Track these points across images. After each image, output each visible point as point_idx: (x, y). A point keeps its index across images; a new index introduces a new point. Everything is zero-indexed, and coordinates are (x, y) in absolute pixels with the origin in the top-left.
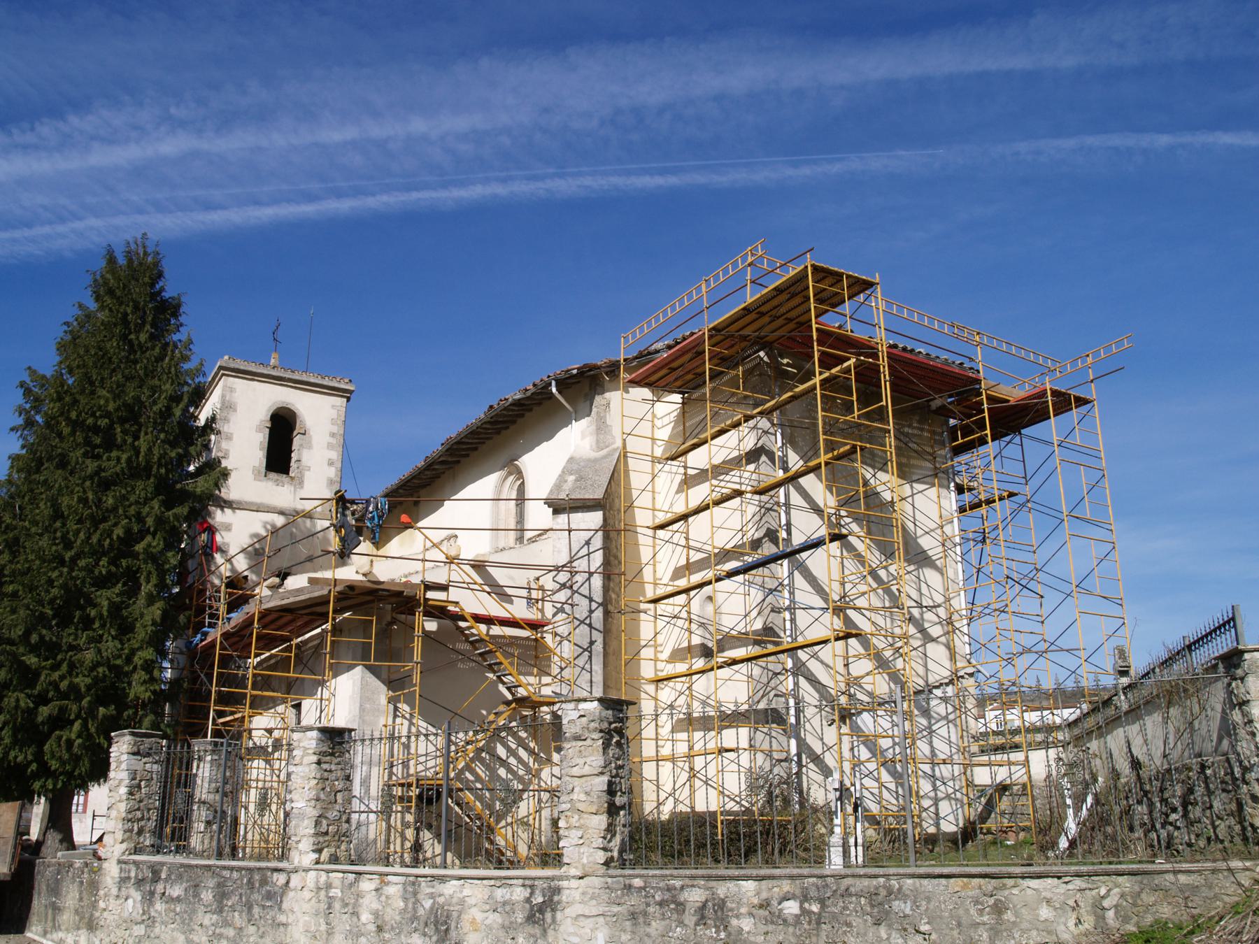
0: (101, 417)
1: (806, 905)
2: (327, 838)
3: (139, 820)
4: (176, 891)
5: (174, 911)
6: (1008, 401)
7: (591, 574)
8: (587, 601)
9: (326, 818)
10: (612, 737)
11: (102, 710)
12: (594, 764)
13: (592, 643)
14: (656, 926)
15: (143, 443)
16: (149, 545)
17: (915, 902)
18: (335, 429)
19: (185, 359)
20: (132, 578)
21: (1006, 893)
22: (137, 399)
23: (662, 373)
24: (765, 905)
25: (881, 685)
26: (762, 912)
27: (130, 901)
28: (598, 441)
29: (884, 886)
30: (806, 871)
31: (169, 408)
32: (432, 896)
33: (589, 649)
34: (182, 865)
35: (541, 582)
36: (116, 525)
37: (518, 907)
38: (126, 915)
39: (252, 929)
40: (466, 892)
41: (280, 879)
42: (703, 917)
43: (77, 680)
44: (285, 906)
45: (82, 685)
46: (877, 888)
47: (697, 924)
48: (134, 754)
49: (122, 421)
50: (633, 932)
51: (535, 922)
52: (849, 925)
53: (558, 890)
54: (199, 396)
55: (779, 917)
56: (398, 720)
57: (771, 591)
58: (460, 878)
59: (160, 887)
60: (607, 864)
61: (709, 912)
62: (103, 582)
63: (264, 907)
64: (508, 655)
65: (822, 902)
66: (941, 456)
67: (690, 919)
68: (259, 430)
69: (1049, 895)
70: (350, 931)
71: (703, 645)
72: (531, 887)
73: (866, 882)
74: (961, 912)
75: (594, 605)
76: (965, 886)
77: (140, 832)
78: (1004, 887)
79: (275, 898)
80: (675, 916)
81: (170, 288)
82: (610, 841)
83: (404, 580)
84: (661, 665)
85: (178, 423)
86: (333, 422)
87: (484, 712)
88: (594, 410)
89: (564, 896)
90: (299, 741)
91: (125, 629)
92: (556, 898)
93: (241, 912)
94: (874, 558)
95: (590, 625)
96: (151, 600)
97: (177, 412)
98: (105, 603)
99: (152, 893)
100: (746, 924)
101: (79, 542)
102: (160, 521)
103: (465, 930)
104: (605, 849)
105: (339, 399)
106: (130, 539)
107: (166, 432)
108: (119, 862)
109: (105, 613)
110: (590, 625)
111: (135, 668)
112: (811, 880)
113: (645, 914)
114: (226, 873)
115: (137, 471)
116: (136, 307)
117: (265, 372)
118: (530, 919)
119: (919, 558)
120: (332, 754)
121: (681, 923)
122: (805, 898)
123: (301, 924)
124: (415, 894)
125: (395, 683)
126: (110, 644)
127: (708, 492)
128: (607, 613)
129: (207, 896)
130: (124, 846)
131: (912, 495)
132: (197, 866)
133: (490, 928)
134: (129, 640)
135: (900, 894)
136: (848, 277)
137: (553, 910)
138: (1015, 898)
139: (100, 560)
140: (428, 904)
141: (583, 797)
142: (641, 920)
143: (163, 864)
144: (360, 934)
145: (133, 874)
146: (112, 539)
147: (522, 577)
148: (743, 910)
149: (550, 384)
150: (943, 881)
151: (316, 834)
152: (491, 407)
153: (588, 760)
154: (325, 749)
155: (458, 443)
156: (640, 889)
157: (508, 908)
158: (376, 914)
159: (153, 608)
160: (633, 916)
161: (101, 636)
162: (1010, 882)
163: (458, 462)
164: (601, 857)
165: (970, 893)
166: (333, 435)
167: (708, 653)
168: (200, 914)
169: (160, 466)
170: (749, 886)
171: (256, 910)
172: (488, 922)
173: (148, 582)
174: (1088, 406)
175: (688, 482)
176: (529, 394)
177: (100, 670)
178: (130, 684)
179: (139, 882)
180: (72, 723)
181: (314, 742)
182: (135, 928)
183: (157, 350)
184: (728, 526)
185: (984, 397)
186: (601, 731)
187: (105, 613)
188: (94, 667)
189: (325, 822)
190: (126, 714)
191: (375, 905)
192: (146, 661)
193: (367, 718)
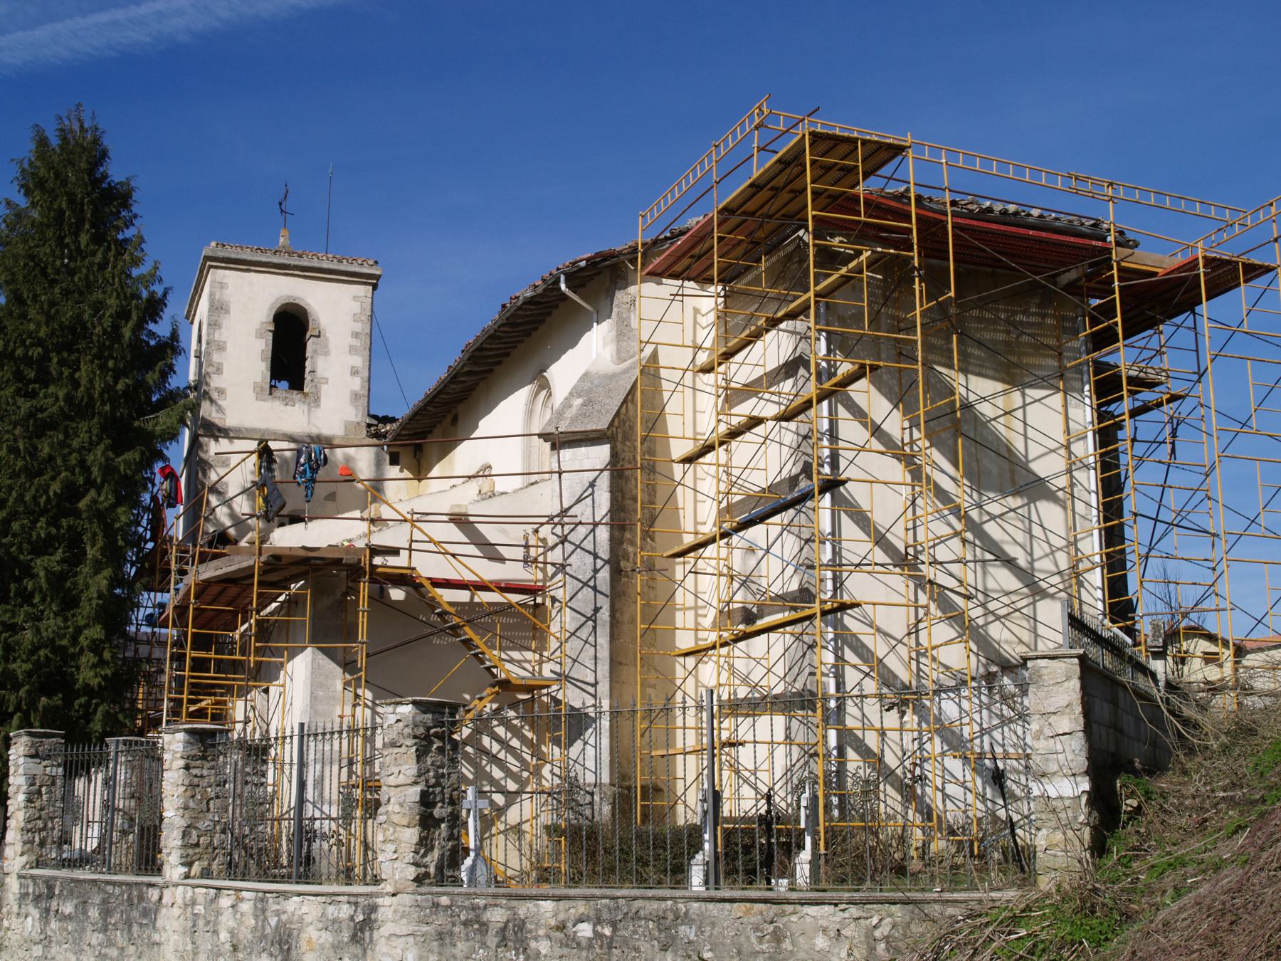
0: (32, 345)
1: (599, 928)
2: (197, 850)
3: (40, 830)
4: (68, 908)
5: (66, 929)
6: (1155, 274)
7: (595, 524)
8: (591, 558)
9: (196, 828)
10: (432, 743)
11: (44, 700)
12: (408, 773)
13: (597, 610)
14: (461, 947)
15: (83, 374)
16: (94, 502)
17: (700, 927)
18: (358, 327)
19: (136, 262)
20: (75, 544)
21: (786, 919)
22: (78, 317)
23: (684, 261)
24: (561, 927)
25: (958, 656)
26: (559, 935)
27: (29, 919)
28: (618, 351)
29: (671, 910)
30: (597, 892)
31: (116, 328)
32: (278, 913)
33: (593, 618)
34: (73, 880)
35: (541, 535)
36: (53, 478)
37: (344, 926)
38: (26, 934)
39: (132, 949)
40: (305, 909)
41: (154, 894)
42: (504, 938)
43: (14, 666)
44: (159, 924)
45: (19, 671)
46: (664, 912)
47: (498, 946)
48: (31, 756)
49: (59, 349)
50: (440, 954)
51: (357, 942)
52: (637, 950)
53: (374, 908)
54: (154, 307)
55: (573, 940)
56: (359, 710)
57: (807, 541)
58: (299, 895)
59: (54, 904)
60: (419, 880)
61: (510, 934)
62: (41, 548)
63: (141, 925)
64: (482, 630)
65: (614, 925)
66: (1072, 349)
67: (492, 941)
68: (259, 335)
69: (823, 922)
70: (211, 950)
71: (744, 608)
72: (356, 904)
73: (655, 905)
74: (743, 939)
75: (599, 563)
76: (748, 912)
77: (42, 844)
78: (783, 913)
79: (150, 914)
80: (478, 937)
81: (116, 172)
82: (424, 856)
83: (346, 544)
84: (701, 634)
85: (130, 345)
86: (356, 318)
87: (467, 697)
88: (615, 310)
89: (381, 915)
90: (169, 743)
91: (69, 603)
92: (373, 916)
93: (122, 931)
94: (962, 493)
95: (595, 588)
96: (98, 567)
97: (127, 333)
98: (42, 574)
99: (47, 910)
100: (543, 947)
101: (11, 500)
102: (108, 469)
103: (303, 950)
104: (416, 864)
105: (362, 287)
106: (72, 493)
107: (116, 359)
108: (20, 877)
109: (44, 586)
110: (595, 588)
111: (82, 650)
112: (604, 901)
113: (451, 934)
114: (110, 889)
115: (78, 409)
116: (72, 201)
117: (264, 259)
118: (355, 939)
119: (1035, 488)
120: (204, 758)
121: (484, 945)
122: (598, 921)
123: (171, 944)
124: (264, 911)
125: (348, 665)
126: (51, 622)
127: (713, 423)
128: (617, 573)
129: (94, 913)
130: (24, 859)
131: (1024, 406)
132: (85, 881)
133: (322, 947)
134: (73, 616)
135: (686, 919)
136: (864, 142)
137: (371, 929)
138: (794, 926)
139: (37, 521)
140: (273, 921)
141: (397, 808)
142: (448, 940)
143: (56, 878)
144: (219, 954)
145: (31, 890)
146: (48, 497)
147: (516, 533)
148: (541, 932)
149: (557, 281)
150: (727, 905)
151: (184, 846)
152: (504, 306)
153: (403, 769)
154: (194, 752)
155: (480, 349)
156: (447, 907)
157: (336, 926)
158: (232, 933)
159: (100, 576)
160: (440, 936)
161: (42, 612)
162: (789, 908)
163: (492, 371)
164: (412, 872)
165: (752, 920)
166: (356, 335)
167: (745, 623)
168: (89, 933)
169: (103, 403)
170: (548, 906)
171: (135, 928)
172: (322, 941)
173: (93, 546)
174: (1271, 274)
175: (733, 396)
176: (539, 290)
177: (42, 652)
178: (78, 668)
179: (37, 899)
180: (11, 716)
181: (181, 745)
182: (35, 948)
183: (99, 255)
184: (766, 460)
185: (1115, 271)
186: (415, 737)
187: (44, 586)
188: (34, 650)
189: (194, 833)
190: (77, 702)
191: (232, 924)
192: (94, 641)
193: (320, 707)
